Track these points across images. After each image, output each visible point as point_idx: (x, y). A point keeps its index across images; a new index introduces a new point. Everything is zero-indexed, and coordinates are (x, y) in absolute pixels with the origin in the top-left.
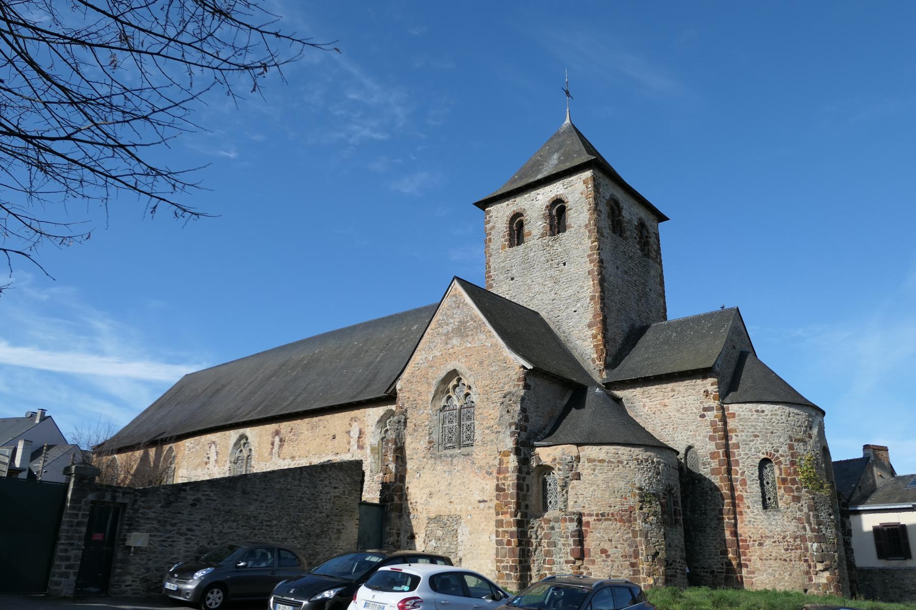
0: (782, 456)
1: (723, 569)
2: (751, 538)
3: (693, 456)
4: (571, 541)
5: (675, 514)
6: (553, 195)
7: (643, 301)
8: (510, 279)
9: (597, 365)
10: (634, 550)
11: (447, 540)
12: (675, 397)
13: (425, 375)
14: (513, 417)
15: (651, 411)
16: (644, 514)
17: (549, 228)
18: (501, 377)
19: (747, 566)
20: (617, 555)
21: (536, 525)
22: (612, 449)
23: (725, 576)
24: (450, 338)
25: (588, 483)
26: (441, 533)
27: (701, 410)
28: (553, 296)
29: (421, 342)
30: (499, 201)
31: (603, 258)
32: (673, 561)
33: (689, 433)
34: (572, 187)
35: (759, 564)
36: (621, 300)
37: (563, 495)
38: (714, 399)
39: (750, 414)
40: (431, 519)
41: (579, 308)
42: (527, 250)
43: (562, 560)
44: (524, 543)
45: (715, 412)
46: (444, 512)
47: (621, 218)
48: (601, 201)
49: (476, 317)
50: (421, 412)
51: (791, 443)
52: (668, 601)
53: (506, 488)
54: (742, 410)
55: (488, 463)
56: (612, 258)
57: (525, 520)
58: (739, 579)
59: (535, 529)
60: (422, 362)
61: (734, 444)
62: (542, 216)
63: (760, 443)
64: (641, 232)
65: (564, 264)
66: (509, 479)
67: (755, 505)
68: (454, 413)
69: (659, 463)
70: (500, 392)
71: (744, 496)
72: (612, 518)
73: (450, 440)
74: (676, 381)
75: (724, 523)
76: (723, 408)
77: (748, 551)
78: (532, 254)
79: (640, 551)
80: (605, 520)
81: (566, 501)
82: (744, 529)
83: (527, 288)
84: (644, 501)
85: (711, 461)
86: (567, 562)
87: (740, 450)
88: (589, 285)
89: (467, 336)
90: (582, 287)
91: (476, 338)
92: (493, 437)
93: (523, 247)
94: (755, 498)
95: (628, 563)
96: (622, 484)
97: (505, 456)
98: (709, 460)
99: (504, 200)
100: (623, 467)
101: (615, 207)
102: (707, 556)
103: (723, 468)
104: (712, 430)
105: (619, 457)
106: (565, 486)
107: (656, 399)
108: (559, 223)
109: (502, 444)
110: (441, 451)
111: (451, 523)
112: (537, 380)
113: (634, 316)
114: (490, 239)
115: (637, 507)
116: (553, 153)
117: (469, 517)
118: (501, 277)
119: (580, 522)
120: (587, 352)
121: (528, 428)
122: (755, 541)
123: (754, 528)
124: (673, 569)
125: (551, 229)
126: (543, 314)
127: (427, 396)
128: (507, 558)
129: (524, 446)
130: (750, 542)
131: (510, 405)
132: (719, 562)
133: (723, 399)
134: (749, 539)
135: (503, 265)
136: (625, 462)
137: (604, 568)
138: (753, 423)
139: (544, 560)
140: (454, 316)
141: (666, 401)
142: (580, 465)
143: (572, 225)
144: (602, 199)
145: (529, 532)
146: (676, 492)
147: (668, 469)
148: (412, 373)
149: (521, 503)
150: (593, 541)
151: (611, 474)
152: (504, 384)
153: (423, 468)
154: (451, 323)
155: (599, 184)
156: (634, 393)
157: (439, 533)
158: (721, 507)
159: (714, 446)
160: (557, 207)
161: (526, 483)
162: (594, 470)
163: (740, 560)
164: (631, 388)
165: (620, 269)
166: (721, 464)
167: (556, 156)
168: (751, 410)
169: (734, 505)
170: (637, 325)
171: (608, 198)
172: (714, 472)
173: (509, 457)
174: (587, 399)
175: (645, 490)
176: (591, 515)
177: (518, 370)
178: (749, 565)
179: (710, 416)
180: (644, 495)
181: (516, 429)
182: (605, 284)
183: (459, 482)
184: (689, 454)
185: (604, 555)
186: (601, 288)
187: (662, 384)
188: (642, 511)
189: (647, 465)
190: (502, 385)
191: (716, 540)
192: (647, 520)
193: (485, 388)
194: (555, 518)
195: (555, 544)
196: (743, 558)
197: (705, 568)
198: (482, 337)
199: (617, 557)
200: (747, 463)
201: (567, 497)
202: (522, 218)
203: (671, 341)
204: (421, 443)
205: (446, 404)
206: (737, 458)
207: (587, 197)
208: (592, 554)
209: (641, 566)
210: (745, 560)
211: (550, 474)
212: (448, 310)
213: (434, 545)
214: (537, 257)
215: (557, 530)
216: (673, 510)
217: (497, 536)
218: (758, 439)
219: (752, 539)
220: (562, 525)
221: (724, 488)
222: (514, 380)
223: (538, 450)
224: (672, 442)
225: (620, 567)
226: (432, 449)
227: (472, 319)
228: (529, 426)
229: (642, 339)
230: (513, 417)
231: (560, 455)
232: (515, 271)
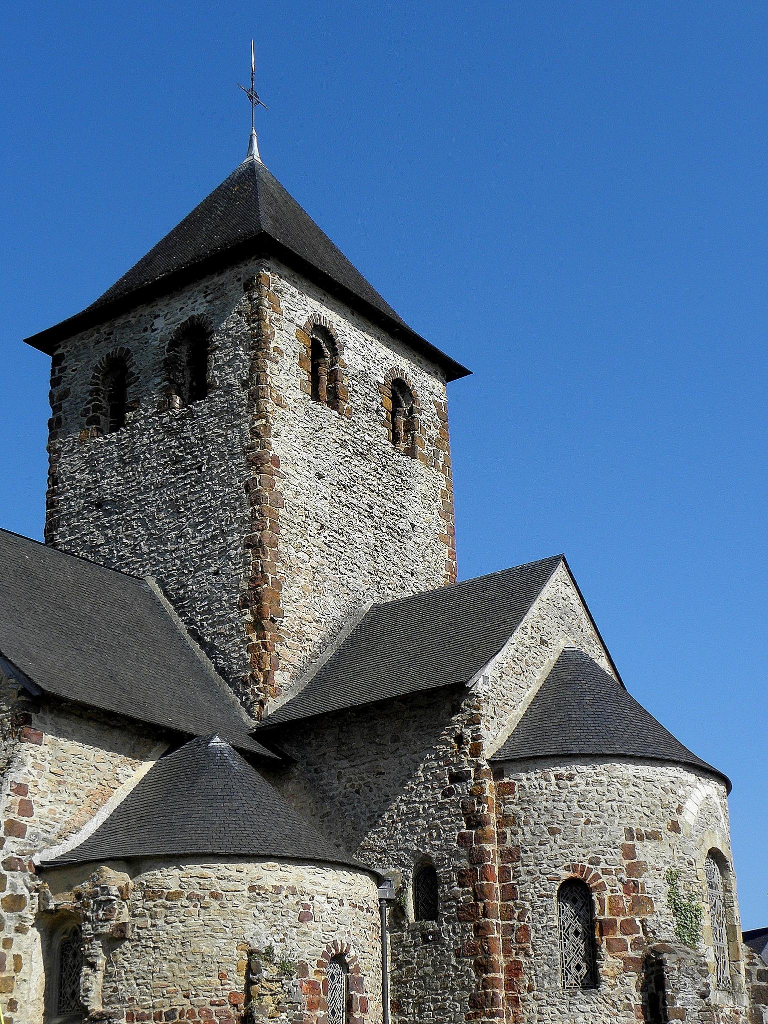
0: (605, 872)
15: (352, 786)
51: (630, 843)
62: (162, 365)
161: (14, 951)
177: (15, 699)
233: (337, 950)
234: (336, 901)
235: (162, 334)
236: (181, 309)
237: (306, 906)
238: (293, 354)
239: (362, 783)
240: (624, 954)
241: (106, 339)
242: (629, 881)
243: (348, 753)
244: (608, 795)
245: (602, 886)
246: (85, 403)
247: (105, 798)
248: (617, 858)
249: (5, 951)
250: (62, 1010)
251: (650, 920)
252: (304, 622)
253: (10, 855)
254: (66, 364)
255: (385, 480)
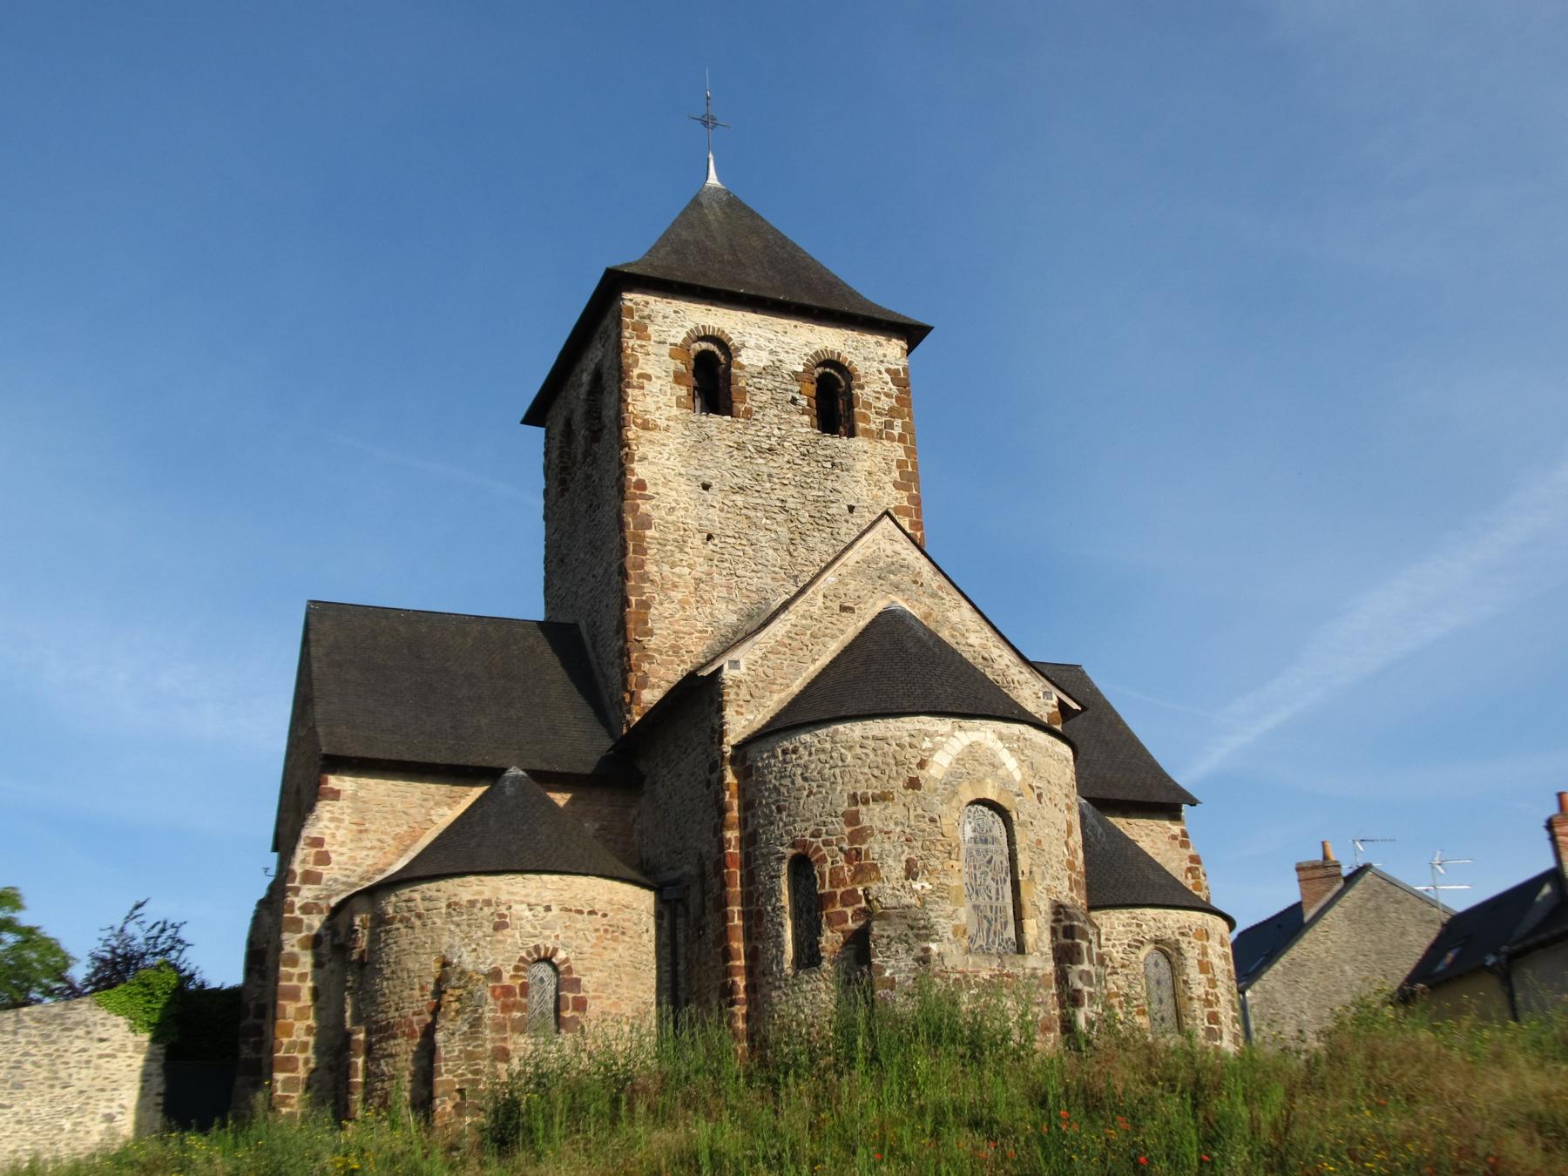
51: (854, 808)
237: (502, 916)
238: (664, 374)
240: (845, 927)
242: (851, 850)
244: (831, 762)
245: (823, 859)
247: (415, 841)
248: (843, 829)
249: (300, 984)
251: (874, 887)
252: (681, 635)
253: (305, 901)
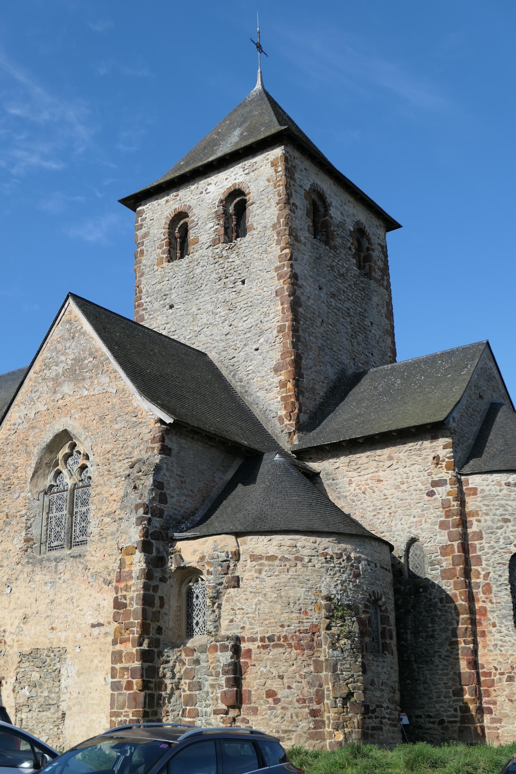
1: (456, 716)
2: (496, 669)
3: (418, 552)
4: (222, 680)
5: (383, 637)
6: (230, 185)
7: (360, 338)
8: (168, 307)
9: (286, 426)
10: (317, 691)
11: (46, 686)
12: (394, 467)
13: (24, 442)
14: (142, 495)
15: (360, 489)
16: (333, 635)
17: (222, 232)
18: (129, 437)
19: (490, 711)
20: (290, 699)
21: (173, 658)
22: (287, 539)
23: (459, 727)
24: (60, 385)
25: (251, 592)
26: (38, 675)
27: (429, 485)
28: (227, 329)
29: (20, 392)
30: (155, 197)
31: (298, 271)
32: (378, 706)
33: (412, 519)
34: (256, 172)
35: (507, 708)
36: (325, 335)
37: (214, 611)
38: (448, 468)
39: (498, 488)
40: (24, 656)
41: (262, 344)
42: (192, 265)
43: (209, 710)
44: (152, 685)
45: (448, 487)
46: (43, 643)
47: (327, 218)
48: (296, 191)
49: (97, 351)
50: (17, 495)
52: (340, 764)
53: (128, 602)
54: (487, 483)
55: (107, 568)
56: (311, 274)
57: (156, 650)
58: (479, 730)
59: (171, 664)
60: (21, 421)
61: (474, 533)
62: (214, 215)
63: (512, 531)
64: (359, 241)
65: (243, 282)
66: (133, 588)
67: (504, 621)
68: (65, 496)
69: (358, 560)
70: (126, 461)
71: (488, 609)
72: (285, 644)
73: (57, 537)
74: (394, 444)
75: (458, 650)
76: (459, 481)
77: (492, 689)
78: (199, 270)
79: (326, 692)
80: (274, 646)
81: (217, 620)
82: (487, 658)
83: (191, 319)
84: (333, 616)
85: (442, 558)
86: (216, 712)
87: (484, 541)
88: (277, 311)
89: (84, 379)
90: (266, 314)
91: (96, 382)
92: (113, 528)
93: (187, 261)
94: (504, 612)
95: (307, 710)
96: (301, 592)
97: (128, 554)
98: (440, 557)
99: (163, 194)
100: (304, 566)
101: (319, 203)
102: (435, 699)
103: (458, 568)
104: (443, 514)
105: (298, 551)
106: (216, 597)
107: (367, 471)
108: (238, 225)
109: (124, 536)
110: (45, 553)
111: (52, 660)
112: (183, 441)
113: (345, 358)
114: (142, 252)
115: (323, 626)
116: (235, 128)
117: (78, 650)
118: (156, 305)
119: (236, 650)
120: (272, 408)
121: (166, 513)
122: (502, 674)
123: (501, 655)
124: (376, 717)
125: (226, 233)
126: (213, 356)
127: (26, 472)
128: (126, 709)
129: (158, 540)
130: (495, 676)
131: (139, 478)
132: (451, 706)
133: (460, 469)
134: (493, 671)
135: (159, 287)
136: (306, 559)
137: (271, 720)
138: (503, 502)
139: (184, 711)
140: (67, 351)
141: (381, 473)
142: (240, 565)
143: (255, 226)
144: (298, 189)
145: (161, 669)
146: (385, 603)
147: (374, 569)
148: (7, 439)
149: (149, 625)
150: (255, 678)
151: (285, 577)
152: (133, 448)
153: (16, 579)
154: (62, 362)
155: (294, 167)
156: (337, 465)
157: (35, 676)
158: (455, 626)
159: (447, 537)
160: (235, 201)
161: (159, 594)
162: (260, 572)
163: (481, 703)
164: (333, 457)
165: (325, 290)
166: (456, 563)
167: (237, 132)
168: (499, 484)
169: (473, 622)
170: (350, 371)
171: (307, 188)
172: (446, 574)
173: (134, 556)
174: (261, 470)
175: (335, 601)
176: (253, 640)
177: (152, 425)
178: (494, 710)
179: (442, 492)
180: (333, 606)
181: (146, 513)
182: (300, 310)
183: (65, 597)
184: (411, 551)
185: (270, 700)
186: (294, 315)
187: (376, 449)
188: (329, 632)
189: (340, 564)
190: (130, 449)
191: (447, 674)
192: (337, 645)
193: (107, 456)
194: (201, 646)
195: (200, 686)
196: (485, 699)
197: (430, 717)
198: (104, 379)
199: (291, 703)
200: (492, 560)
201: (220, 614)
202: (186, 220)
203: (393, 391)
204: (15, 542)
205: (53, 483)
206: (479, 553)
207: (275, 184)
208: (253, 699)
209: (326, 714)
210: (489, 702)
211: (197, 581)
212: (59, 342)
213: (28, 694)
214: (206, 274)
215: (203, 664)
216: (380, 630)
217: (113, 677)
218: (509, 524)
219: (499, 671)
220: (211, 656)
221: (459, 598)
222: (147, 441)
223: (179, 545)
224: (387, 534)
225: (294, 717)
226: (29, 550)
227: (91, 354)
228: (168, 509)
229: (354, 390)
230: (142, 495)
231: (211, 552)
232: (175, 295)
233: (375, 597)
234: (373, 565)
235: (213, 195)
236: (226, 179)
239: (367, 487)
241: (173, 199)
243: (356, 467)
246: (160, 240)
250: (189, 634)
252: (315, 382)
254: (146, 216)
255: (356, 293)
